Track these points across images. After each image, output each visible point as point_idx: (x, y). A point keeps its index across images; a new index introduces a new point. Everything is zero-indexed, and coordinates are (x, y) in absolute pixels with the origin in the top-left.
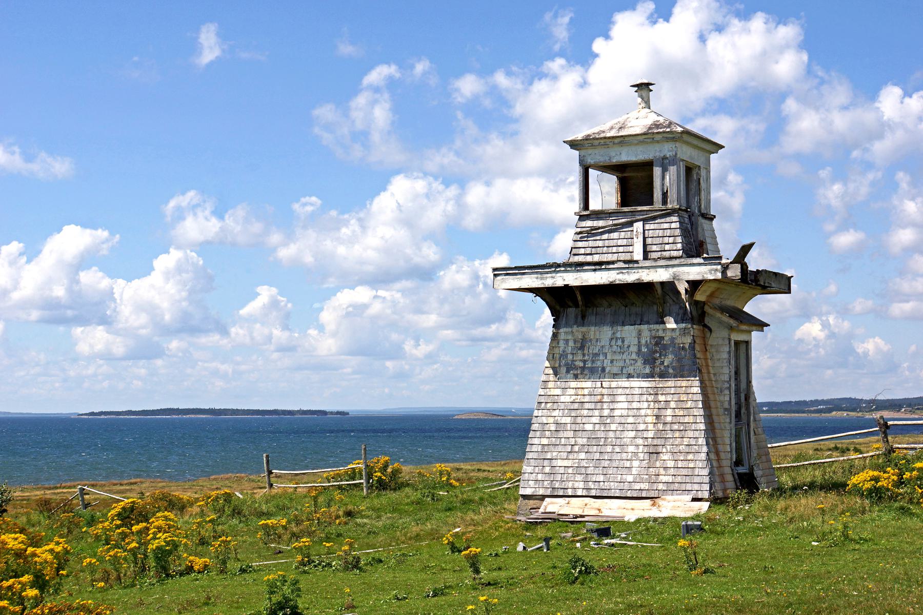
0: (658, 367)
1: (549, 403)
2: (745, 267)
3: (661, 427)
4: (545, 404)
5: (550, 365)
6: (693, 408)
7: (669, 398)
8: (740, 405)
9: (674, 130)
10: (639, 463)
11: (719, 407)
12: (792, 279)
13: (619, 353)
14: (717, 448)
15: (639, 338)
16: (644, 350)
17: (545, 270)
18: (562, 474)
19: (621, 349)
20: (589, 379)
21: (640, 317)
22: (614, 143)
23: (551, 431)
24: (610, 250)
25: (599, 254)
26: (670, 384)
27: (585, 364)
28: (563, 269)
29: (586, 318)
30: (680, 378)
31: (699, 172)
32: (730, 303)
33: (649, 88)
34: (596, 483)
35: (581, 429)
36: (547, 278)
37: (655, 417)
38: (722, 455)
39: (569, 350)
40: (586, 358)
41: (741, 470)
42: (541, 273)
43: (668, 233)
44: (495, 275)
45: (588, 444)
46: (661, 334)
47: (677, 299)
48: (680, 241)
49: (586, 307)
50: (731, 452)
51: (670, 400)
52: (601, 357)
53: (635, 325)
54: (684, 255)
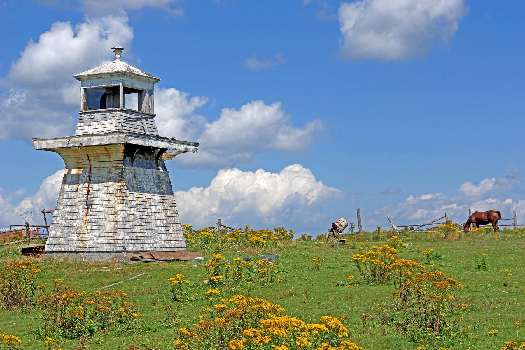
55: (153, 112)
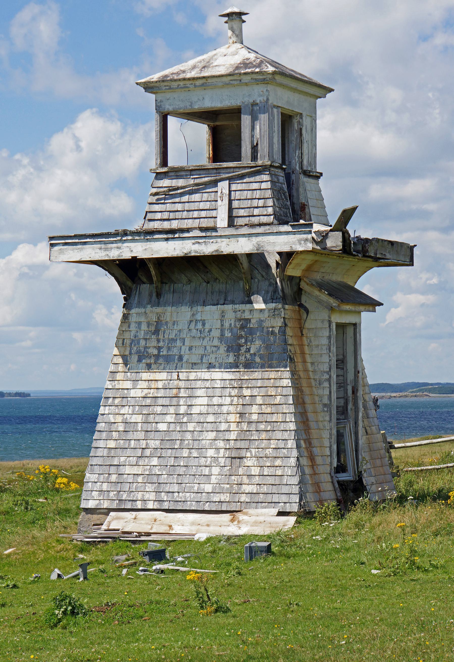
0: (243, 355)
1: (117, 398)
2: (346, 235)
3: (245, 426)
4: (113, 399)
5: (120, 353)
6: (282, 404)
7: (255, 392)
8: (347, 399)
9: (264, 70)
10: (219, 470)
11: (317, 402)
12: (415, 249)
13: (199, 338)
14: (311, 452)
15: (222, 321)
16: (228, 334)
17: (110, 239)
18: (130, 483)
19: (201, 333)
20: (164, 369)
21: (224, 295)
22: (195, 86)
23: (119, 431)
24: (191, 214)
25: (178, 219)
26: (257, 375)
27: (159, 352)
28: (130, 238)
29: (162, 297)
30: (268, 368)
31: (301, 120)
32: (336, 278)
33: (241, 18)
34: (170, 494)
35: (153, 429)
36: (111, 248)
37: (238, 415)
38: (319, 460)
39: (141, 335)
40: (161, 344)
41: (343, 477)
42: (105, 243)
43: (258, 194)
44: (52, 245)
45: (161, 447)
46: (247, 315)
47: (267, 274)
48: (271, 204)
49: (162, 283)
50: (331, 456)
51: (256, 394)
52: (179, 343)
53: (217, 304)
54: (276, 222)
55: (315, 167)
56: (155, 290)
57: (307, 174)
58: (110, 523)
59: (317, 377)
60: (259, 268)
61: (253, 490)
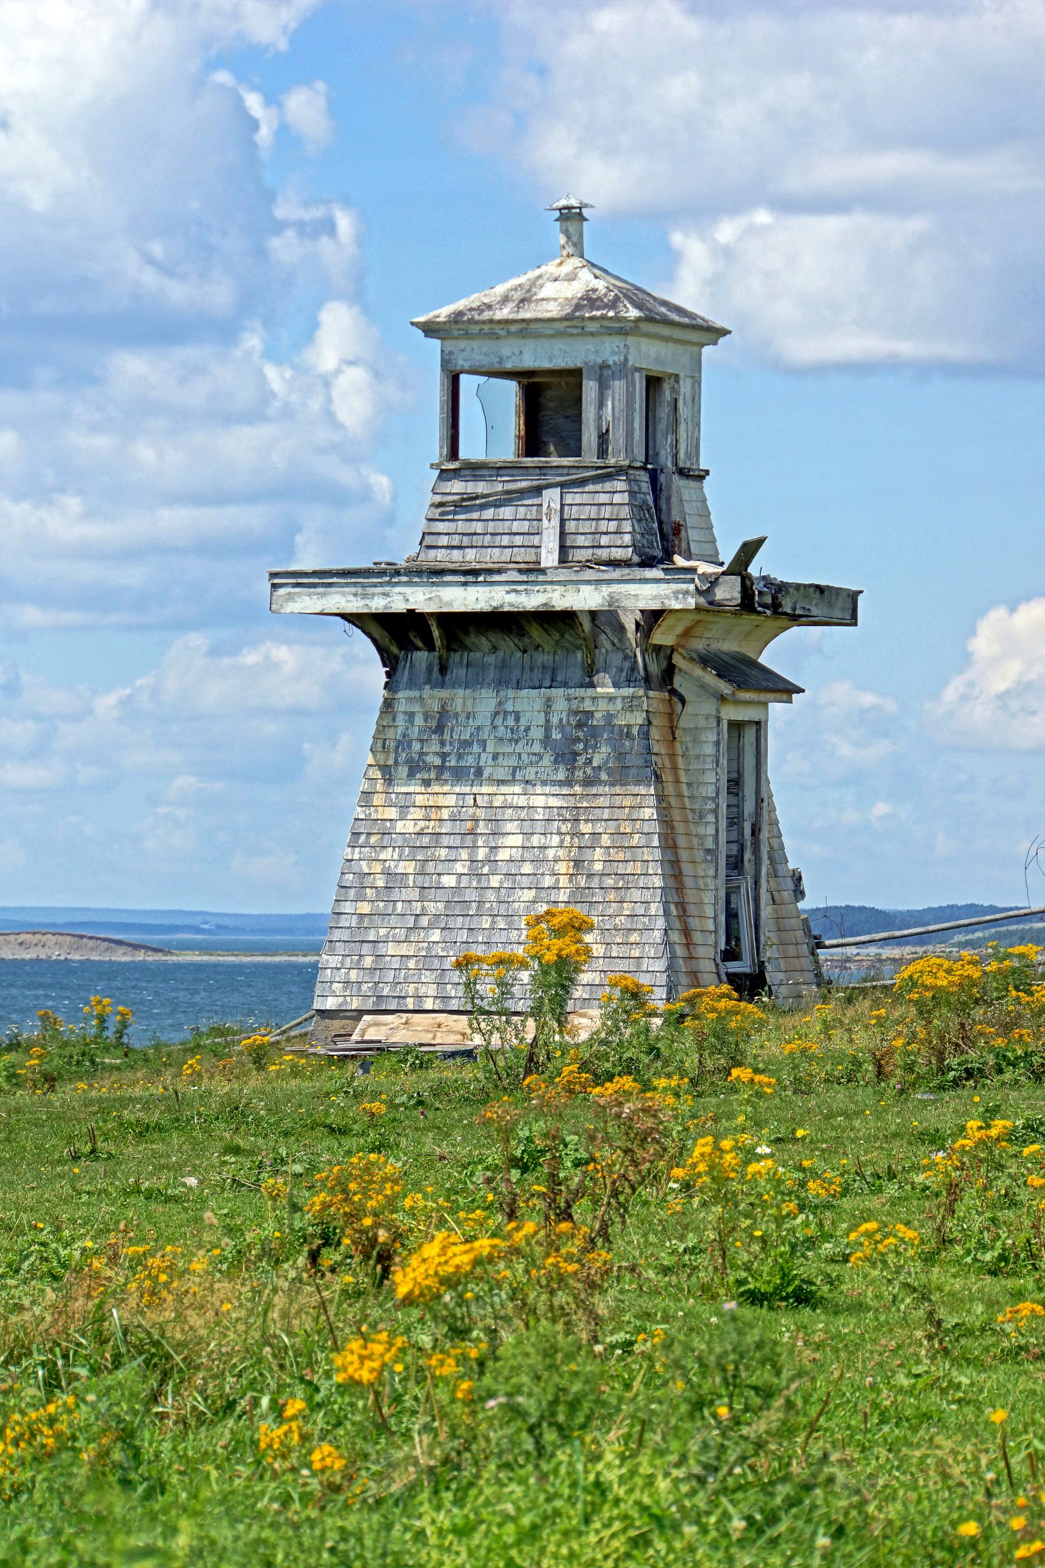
2: (748, 582)
3: (582, 882)
7: (599, 828)
15: (547, 714)
16: (556, 735)
22: (508, 332)
27: (444, 761)
28: (404, 579)
32: (729, 646)
36: (374, 595)
38: (697, 938)
39: (415, 732)
41: (734, 967)
42: (363, 586)
43: (606, 511)
44: (274, 586)
46: (588, 706)
47: (621, 640)
48: (629, 529)
52: (476, 748)
55: (698, 460)
56: (436, 662)
57: (683, 473)
58: (364, 1031)
59: (696, 806)
60: (608, 630)
61: (594, 980)
